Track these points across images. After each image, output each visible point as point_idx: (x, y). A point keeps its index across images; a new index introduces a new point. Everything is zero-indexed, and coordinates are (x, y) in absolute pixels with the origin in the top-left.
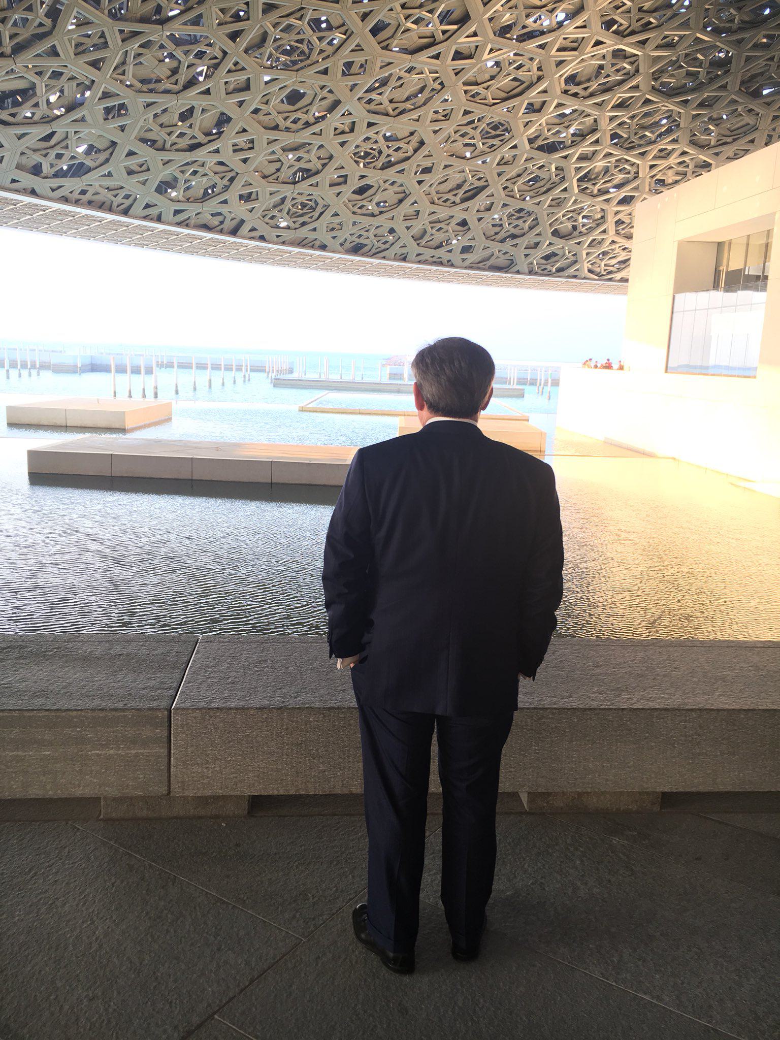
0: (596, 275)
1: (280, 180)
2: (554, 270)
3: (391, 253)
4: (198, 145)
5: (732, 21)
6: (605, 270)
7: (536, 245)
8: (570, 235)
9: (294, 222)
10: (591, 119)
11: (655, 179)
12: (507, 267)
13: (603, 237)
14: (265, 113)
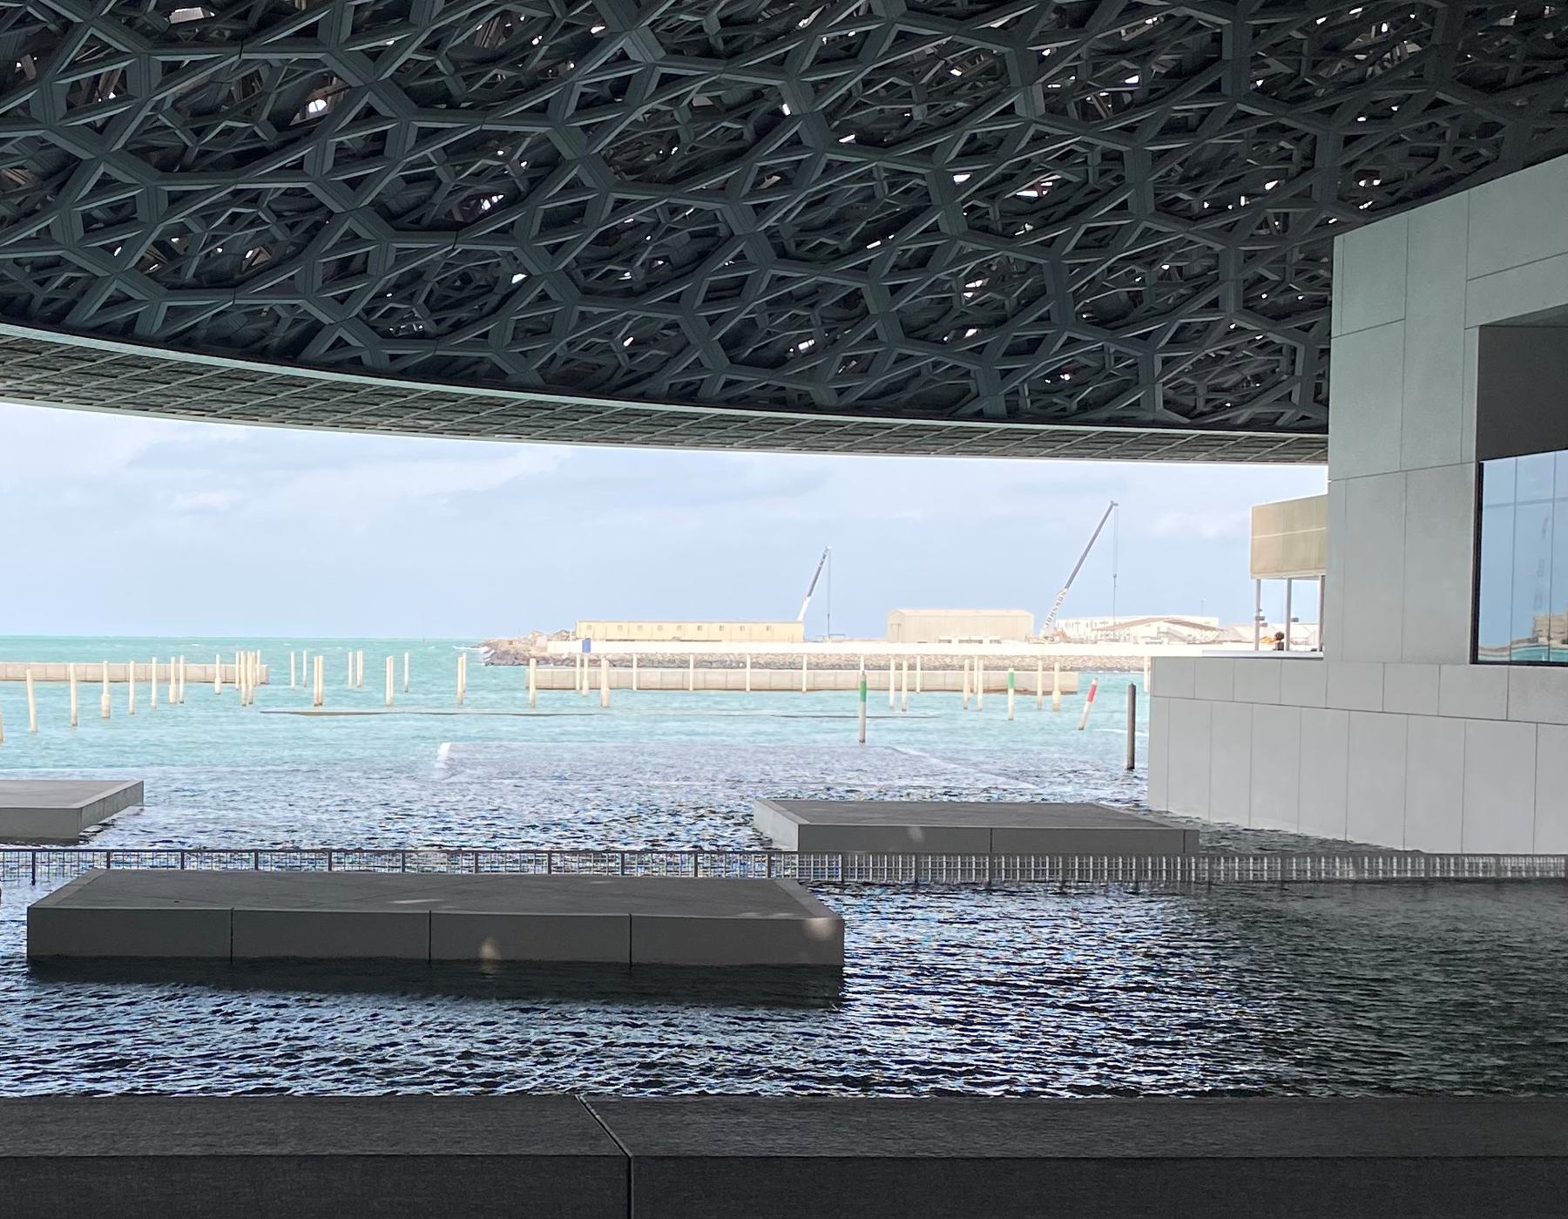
0: (1184, 415)
1: (426, 221)
2: (1074, 406)
3: (663, 382)
4: (260, 154)
5: (1289, 159)
6: (1208, 401)
7: (1033, 346)
8: (1124, 316)
9: (438, 322)
10: (1205, 37)
11: (1354, 171)
12: (947, 406)
13: (1411, 92)
14: (564, 359)
